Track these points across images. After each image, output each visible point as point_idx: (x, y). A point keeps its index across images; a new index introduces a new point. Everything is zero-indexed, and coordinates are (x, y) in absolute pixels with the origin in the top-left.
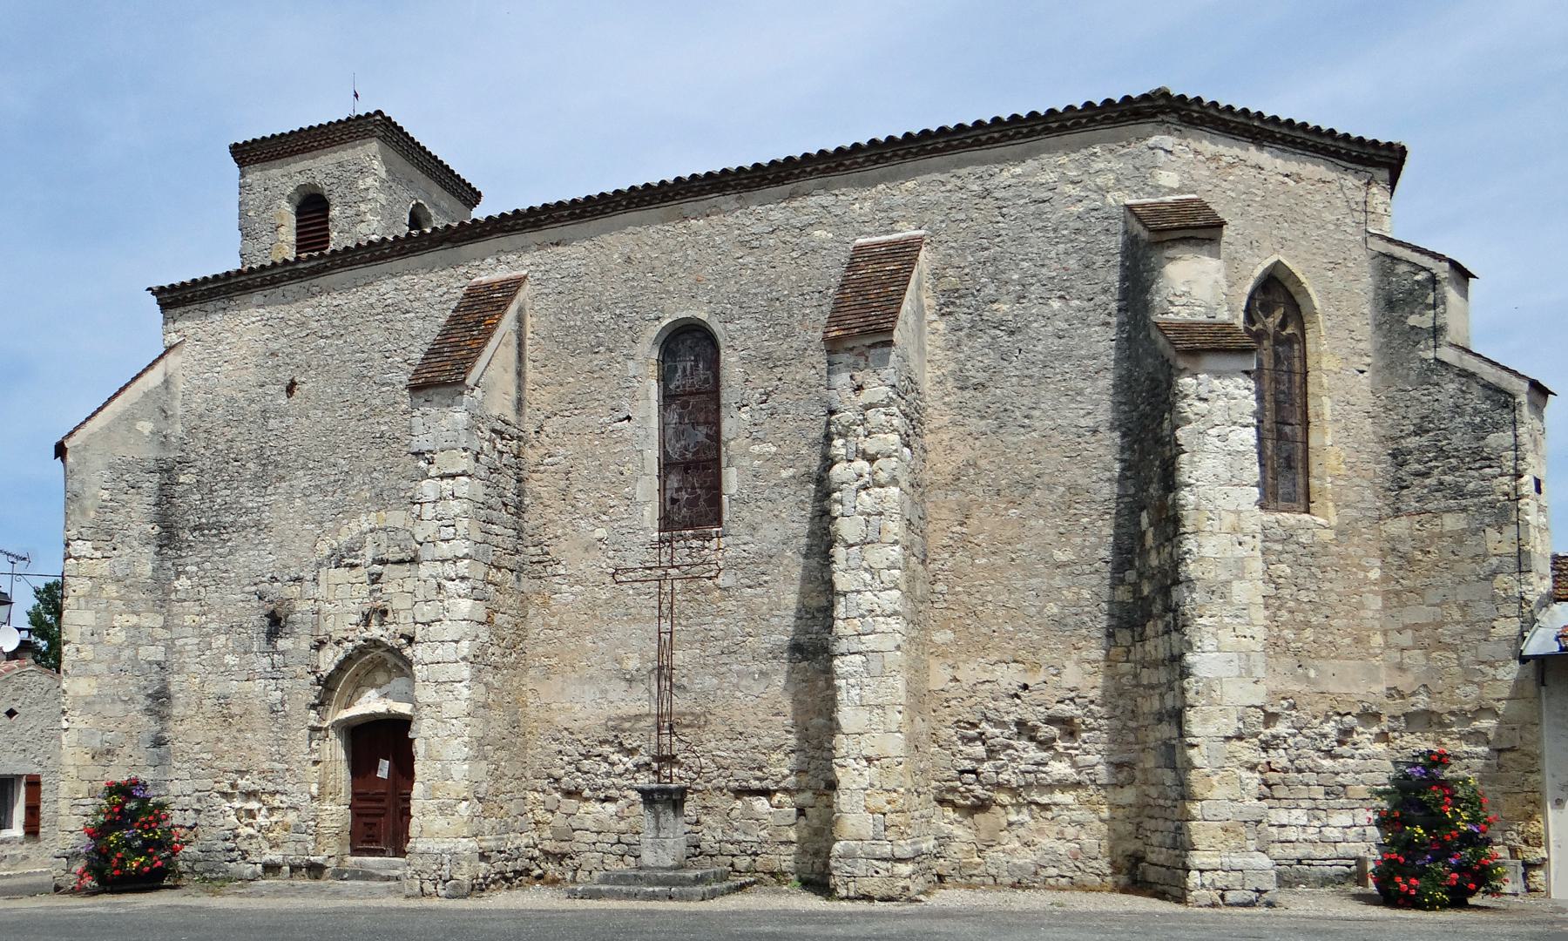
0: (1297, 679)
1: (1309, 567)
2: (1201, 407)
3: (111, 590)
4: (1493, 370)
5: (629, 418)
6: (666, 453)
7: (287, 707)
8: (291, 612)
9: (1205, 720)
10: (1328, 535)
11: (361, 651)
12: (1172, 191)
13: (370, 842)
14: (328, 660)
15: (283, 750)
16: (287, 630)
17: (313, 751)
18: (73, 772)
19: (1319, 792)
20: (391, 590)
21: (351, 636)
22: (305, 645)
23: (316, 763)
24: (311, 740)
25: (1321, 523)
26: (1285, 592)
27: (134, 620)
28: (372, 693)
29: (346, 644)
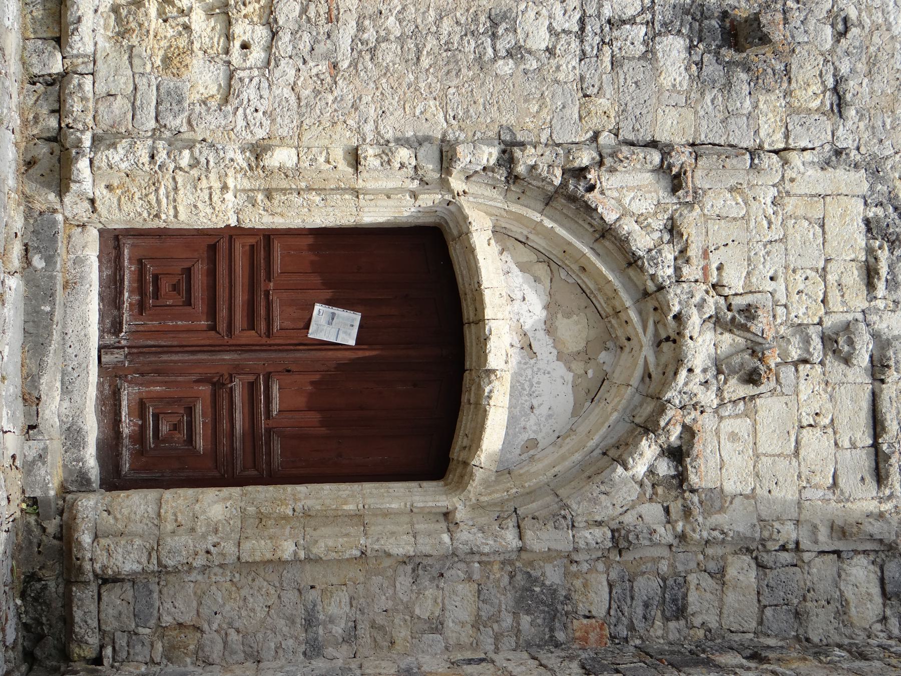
4: (226, 272)
7: (505, 67)
8: (755, 80)
11: (652, 296)
13: (141, 289)
14: (629, 197)
15: (389, 53)
16: (712, 68)
17: (386, 148)
20: (805, 390)
21: (690, 272)
22: (670, 126)
23: (355, 159)
24: (417, 143)
28: (533, 309)
29: (669, 254)
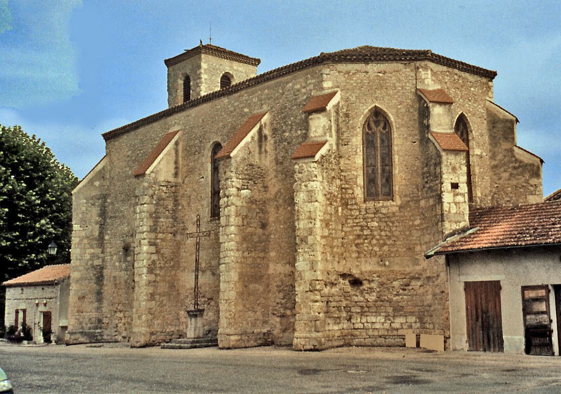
0: (381, 266)
1: (386, 222)
2: (300, 175)
3: (86, 241)
5: (203, 177)
6: (214, 189)
9: (299, 286)
10: (395, 209)
12: (329, 88)
18: (72, 304)
19: (390, 310)
25: (391, 206)
26: (375, 233)
27: (92, 251)
